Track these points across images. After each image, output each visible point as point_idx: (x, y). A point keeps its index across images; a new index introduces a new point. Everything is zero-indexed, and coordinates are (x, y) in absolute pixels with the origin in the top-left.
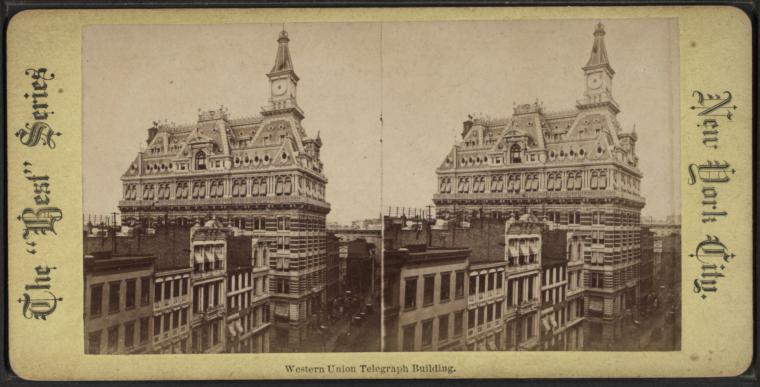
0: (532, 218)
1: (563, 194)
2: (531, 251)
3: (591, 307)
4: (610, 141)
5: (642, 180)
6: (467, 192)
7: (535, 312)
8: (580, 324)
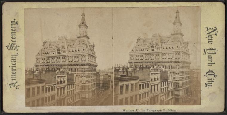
0: (158, 67)
1: (167, 60)
2: (157, 77)
3: (176, 94)
5: (96, 58)
6: (54, 62)
7: (65, 98)
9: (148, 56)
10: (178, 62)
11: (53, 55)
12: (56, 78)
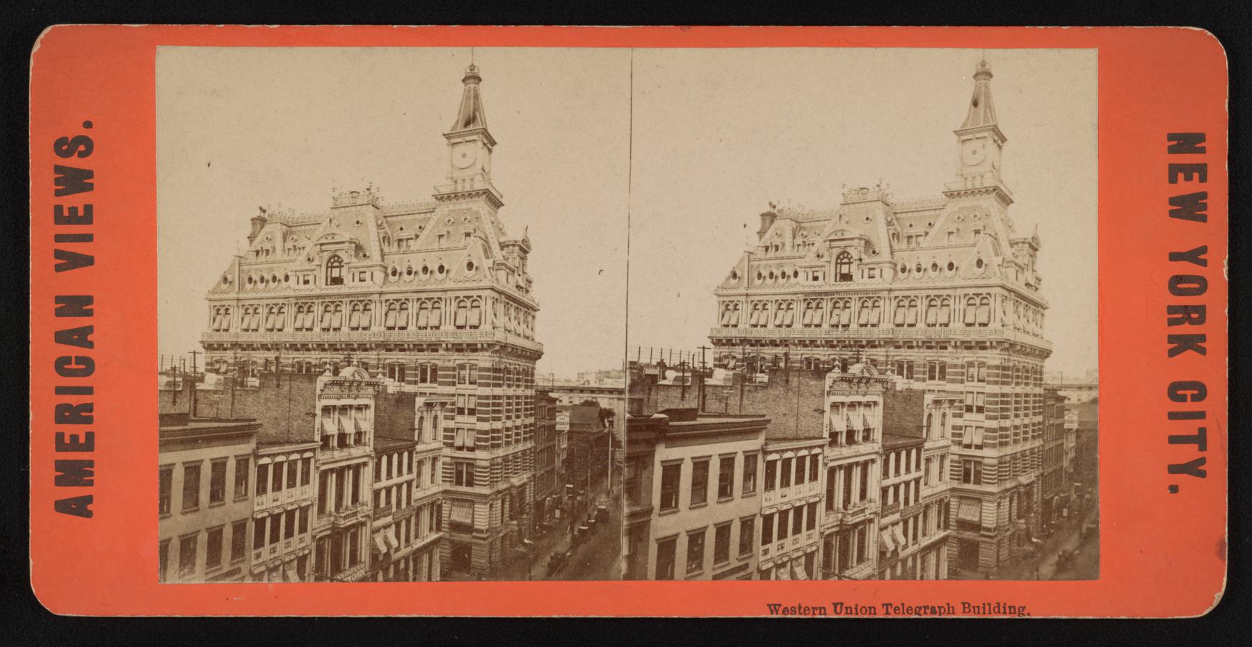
0: (868, 371)
1: (412, 335)
3: (961, 516)
4: (487, 250)
5: (1046, 312)
7: (363, 524)
9: (818, 307)
10: (468, 345)
11: (304, 290)
12: (823, 412)
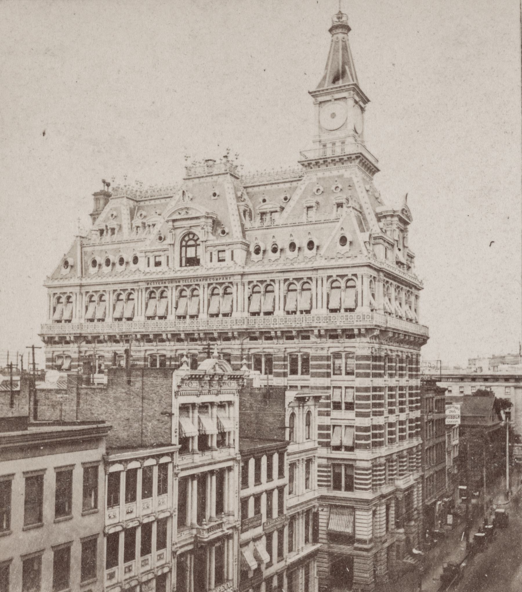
1: (279, 321)
2: (219, 425)
8: (312, 556)
10: (344, 331)
11: (156, 273)
12: (171, 415)
